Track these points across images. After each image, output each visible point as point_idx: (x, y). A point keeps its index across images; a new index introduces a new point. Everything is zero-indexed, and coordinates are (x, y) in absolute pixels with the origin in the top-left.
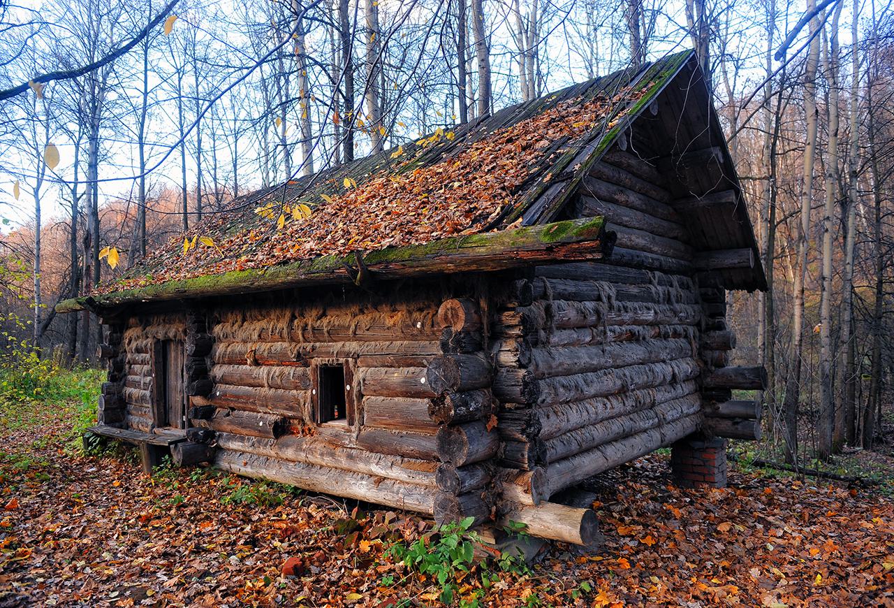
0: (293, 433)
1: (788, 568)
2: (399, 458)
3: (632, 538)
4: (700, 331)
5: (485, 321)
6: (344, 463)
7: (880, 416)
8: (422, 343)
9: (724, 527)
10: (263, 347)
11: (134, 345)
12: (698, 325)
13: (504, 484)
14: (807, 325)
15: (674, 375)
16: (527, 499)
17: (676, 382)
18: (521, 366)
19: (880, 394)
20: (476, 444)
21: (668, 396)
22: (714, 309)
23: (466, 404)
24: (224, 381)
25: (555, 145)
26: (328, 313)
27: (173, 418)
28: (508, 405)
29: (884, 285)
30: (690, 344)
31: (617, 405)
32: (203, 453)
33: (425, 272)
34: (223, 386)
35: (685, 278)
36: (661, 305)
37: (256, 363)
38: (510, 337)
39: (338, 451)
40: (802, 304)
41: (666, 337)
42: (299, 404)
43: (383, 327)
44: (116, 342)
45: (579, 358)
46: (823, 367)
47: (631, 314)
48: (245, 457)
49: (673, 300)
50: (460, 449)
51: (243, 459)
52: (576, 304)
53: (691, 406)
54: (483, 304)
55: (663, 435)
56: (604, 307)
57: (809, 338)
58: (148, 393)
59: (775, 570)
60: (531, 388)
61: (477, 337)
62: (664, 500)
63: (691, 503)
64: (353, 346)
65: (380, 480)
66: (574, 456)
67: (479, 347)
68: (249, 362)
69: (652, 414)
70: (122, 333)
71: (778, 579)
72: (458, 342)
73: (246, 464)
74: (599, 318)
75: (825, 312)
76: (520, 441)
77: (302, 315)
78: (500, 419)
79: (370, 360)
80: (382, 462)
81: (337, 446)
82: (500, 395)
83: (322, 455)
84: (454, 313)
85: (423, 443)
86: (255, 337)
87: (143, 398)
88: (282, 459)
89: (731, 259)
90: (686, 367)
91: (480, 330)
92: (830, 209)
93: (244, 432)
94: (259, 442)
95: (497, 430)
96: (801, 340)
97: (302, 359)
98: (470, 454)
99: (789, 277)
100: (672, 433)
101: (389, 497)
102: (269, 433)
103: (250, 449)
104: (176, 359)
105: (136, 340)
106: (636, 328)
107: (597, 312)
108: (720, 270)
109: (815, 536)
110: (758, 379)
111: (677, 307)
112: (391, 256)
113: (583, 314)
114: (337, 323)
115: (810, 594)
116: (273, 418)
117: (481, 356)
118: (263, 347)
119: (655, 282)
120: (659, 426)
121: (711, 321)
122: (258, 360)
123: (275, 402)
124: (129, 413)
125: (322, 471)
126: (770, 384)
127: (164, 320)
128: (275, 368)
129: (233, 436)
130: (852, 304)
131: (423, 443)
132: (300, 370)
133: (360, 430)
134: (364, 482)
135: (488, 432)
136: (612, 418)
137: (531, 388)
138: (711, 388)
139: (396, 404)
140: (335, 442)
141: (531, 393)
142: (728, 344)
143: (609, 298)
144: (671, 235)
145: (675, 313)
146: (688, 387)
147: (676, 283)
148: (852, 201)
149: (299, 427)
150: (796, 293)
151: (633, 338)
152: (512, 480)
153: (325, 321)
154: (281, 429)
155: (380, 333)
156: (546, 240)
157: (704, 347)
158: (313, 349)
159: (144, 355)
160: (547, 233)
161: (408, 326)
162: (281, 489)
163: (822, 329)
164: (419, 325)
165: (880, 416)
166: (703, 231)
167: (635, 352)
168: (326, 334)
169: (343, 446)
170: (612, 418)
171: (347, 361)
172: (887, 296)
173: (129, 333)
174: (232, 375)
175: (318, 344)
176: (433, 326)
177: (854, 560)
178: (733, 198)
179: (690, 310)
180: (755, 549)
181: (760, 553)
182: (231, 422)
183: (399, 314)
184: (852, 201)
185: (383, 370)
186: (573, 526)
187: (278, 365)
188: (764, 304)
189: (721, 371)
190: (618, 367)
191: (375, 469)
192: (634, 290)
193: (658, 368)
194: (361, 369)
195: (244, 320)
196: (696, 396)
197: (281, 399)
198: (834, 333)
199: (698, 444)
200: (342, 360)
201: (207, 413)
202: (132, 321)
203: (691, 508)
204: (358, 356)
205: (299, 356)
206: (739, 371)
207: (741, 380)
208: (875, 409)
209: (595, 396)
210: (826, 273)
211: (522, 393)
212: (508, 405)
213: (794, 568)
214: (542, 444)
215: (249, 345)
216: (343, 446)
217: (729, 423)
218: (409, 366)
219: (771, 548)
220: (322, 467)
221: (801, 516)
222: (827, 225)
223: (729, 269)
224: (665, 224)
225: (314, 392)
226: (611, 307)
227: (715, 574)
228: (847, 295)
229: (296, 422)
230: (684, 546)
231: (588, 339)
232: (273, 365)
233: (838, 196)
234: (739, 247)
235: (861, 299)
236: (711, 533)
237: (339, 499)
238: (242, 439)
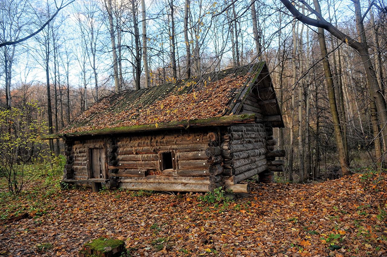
0: (151, 175)
1: (295, 197)
2: (192, 177)
3: (256, 194)
4: (266, 140)
5: (219, 138)
6: (173, 181)
7: (319, 170)
8: (199, 145)
9: (278, 190)
10: (140, 149)
11: (78, 150)
12: (265, 138)
13: (226, 180)
14: (295, 137)
15: (260, 153)
16: (232, 183)
17: (260, 155)
18: (229, 149)
19: (319, 162)
20: (219, 169)
21: (258, 159)
22: (269, 132)
23: (217, 159)
24: (122, 160)
25: (233, 90)
26: (165, 137)
27: (96, 175)
28: (226, 160)
29: (319, 123)
30: (263, 144)
31: (247, 161)
32: (116, 185)
33: (207, 126)
34: (122, 162)
35: (261, 124)
36: (257, 132)
37: (137, 154)
38: (226, 142)
39: (170, 178)
40: (293, 131)
41: (257, 142)
42: (155, 165)
43: (186, 141)
44: (70, 150)
45: (238, 148)
46: (300, 152)
47: (249, 135)
48: (130, 184)
49: (259, 131)
50: (216, 171)
51: (132, 185)
52: (237, 133)
53: (264, 162)
54: (219, 133)
55: (258, 170)
56: (243, 134)
57: (296, 143)
58: (86, 167)
59: (292, 198)
60: (232, 154)
61: (217, 142)
62: (261, 186)
63: (269, 186)
64: (175, 147)
65: (185, 184)
66: (238, 175)
67: (218, 145)
68: (134, 153)
69: (255, 164)
70: (72, 146)
71: (293, 200)
72: (213, 144)
73: (133, 186)
74: (242, 137)
75: (300, 133)
76: (229, 169)
77: (155, 138)
78: (224, 163)
79: (181, 150)
80: (186, 179)
81: (170, 176)
82: (224, 157)
83: (164, 179)
84: (212, 136)
85: (200, 172)
86: (136, 145)
87: (83, 169)
88: (148, 183)
89: (274, 118)
90: (263, 151)
91: (218, 140)
92: (301, 98)
93: (132, 176)
94: (139, 178)
95: (223, 166)
96: (293, 143)
97: (155, 151)
98: (218, 172)
99: (288, 121)
100: (261, 170)
101: (189, 189)
102: (143, 175)
103: (135, 181)
104: (97, 155)
105: (77, 148)
106: (251, 139)
107: (242, 135)
108: (271, 122)
109: (301, 191)
110: (283, 154)
111: (260, 133)
112: (197, 122)
113: (239, 135)
114: (169, 140)
115: (300, 201)
116: (144, 170)
117: (219, 147)
118: (140, 149)
119: (254, 126)
120: (257, 168)
121: (269, 137)
122: (135, 153)
123: (146, 165)
124: (75, 175)
125: (164, 184)
126: (286, 154)
127: (93, 142)
128: (144, 155)
129: (127, 177)
130: (309, 130)
131: (200, 172)
132: (154, 155)
133: (178, 171)
134: (180, 186)
135: (221, 167)
136: (246, 165)
137: (232, 154)
138: (269, 158)
139: (190, 162)
140: (169, 175)
141: (232, 156)
142: (274, 144)
143: (245, 131)
144: (258, 112)
145: (260, 135)
146: (263, 157)
147: (259, 126)
148: (308, 95)
149: (153, 172)
150: (291, 127)
151: (250, 142)
152: (227, 179)
153: (165, 140)
154: (147, 173)
155: (185, 142)
156: (242, 119)
157: (267, 145)
158: (160, 148)
159: (83, 154)
160: (241, 117)
161: (194, 140)
162: (149, 192)
163: (300, 138)
164: (198, 140)
165: (319, 170)
166: (266, 110)
167: (250, 146)
168: (165, 144)
169: (172, 176)
170: (246, 165)
171: (173, 151)
172: (321, 127)
173: (74, 147)
174: (126, 158)
175: (161, 147)
176: (203, 140)
177: (310, 194)
178: (275, 101)
179: (263, 134)
180: (286, 194)
181: (288, 195)
182: (126, 173)
183: (191, 137)
184: (308, 95)
185: (186, 153)
186: (245, 188)
187: (145, 154)
188: (280, 131)
189: (272, 152)
190: (247, 150)
191: (184, 181)
192: (250, 128)
193: (256, 151)
194: (178, 153)
195: (130, 141)
196: (265, 159)
197: (148, 164)
198: (303, 140)
199: (266, 174)
200: (171, 151)
201: (116, 171)
202: (76, 142)
203: (269, 187)
204: (177, 149)
205: (154, 150)
206: (277, 151)
207: (278, 154)
208: (317, 167)
209: (242, 158)
210: (300, 120)
211: (230, 156)
212: (226, 160)
213: (296, 197)
214: (235, 169)
215: (133, 148)
216: (172, 176)
217: (275, 167)
218: (194, 151)
219: (290, 194)
220: (163, 183)
221: (297, 187)
222: (300, 103)
223: (274, 121)
224: (256, 108)
225: (160, 161)
226: (245, 133)
227: (278, 199)
228: (307, 127)
229: (152, 171)
230: (269, 195)
231: (240, 143)
232: (143, 154)
233: (303, 92)
234: (276, 115)
235: (312, 129)
236: (275, 192)
237: (171, 192)
238: (131, 178)
